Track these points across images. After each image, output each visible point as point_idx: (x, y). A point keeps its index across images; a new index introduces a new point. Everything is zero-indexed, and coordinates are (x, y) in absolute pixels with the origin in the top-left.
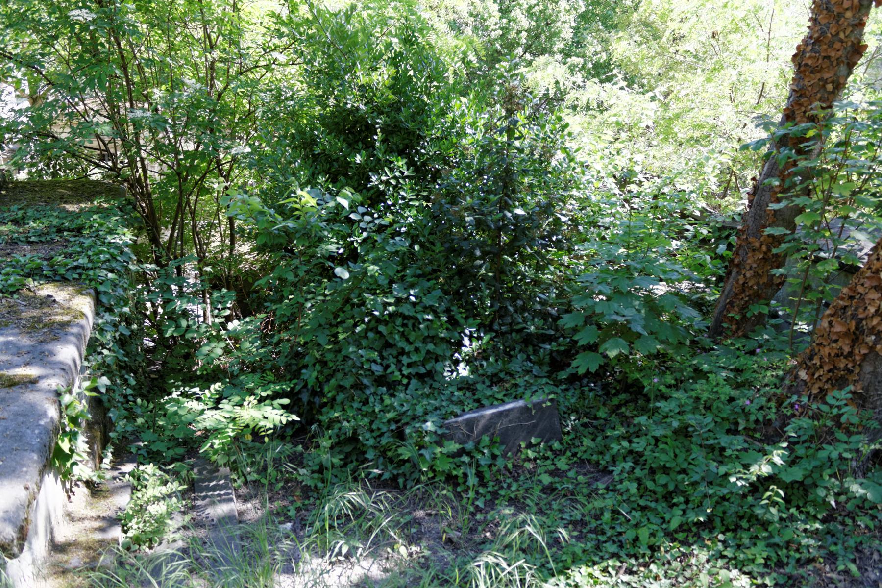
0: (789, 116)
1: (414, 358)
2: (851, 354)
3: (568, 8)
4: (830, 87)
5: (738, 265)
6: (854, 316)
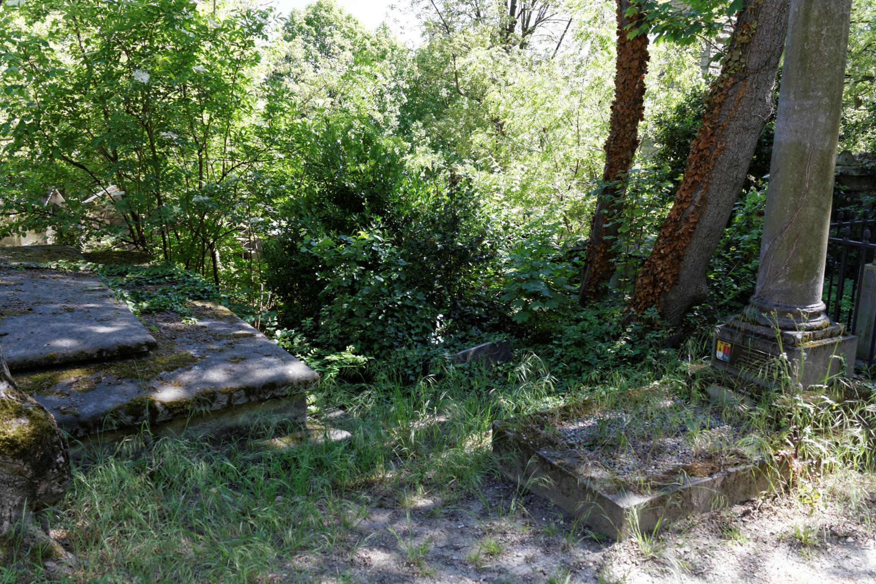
0: (606, 177)
1: (417, 330)
2: (653, 293)
3: (393, 99)
4: (625, 162)
5: (590, 262)
6: (652, 274)
